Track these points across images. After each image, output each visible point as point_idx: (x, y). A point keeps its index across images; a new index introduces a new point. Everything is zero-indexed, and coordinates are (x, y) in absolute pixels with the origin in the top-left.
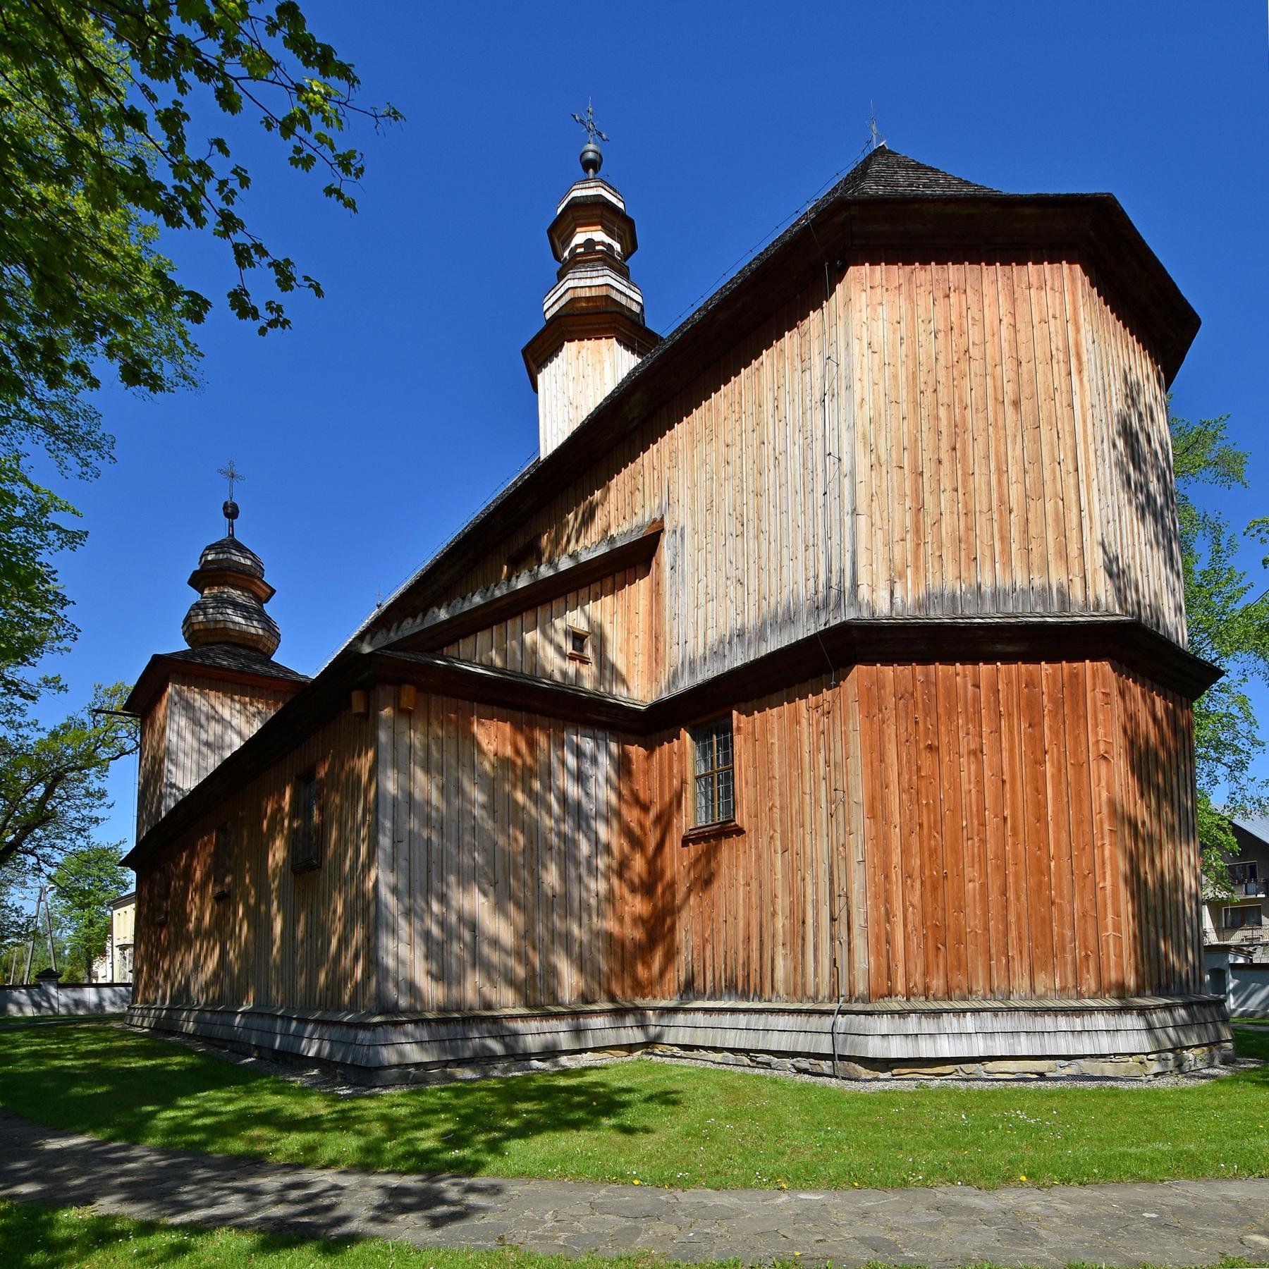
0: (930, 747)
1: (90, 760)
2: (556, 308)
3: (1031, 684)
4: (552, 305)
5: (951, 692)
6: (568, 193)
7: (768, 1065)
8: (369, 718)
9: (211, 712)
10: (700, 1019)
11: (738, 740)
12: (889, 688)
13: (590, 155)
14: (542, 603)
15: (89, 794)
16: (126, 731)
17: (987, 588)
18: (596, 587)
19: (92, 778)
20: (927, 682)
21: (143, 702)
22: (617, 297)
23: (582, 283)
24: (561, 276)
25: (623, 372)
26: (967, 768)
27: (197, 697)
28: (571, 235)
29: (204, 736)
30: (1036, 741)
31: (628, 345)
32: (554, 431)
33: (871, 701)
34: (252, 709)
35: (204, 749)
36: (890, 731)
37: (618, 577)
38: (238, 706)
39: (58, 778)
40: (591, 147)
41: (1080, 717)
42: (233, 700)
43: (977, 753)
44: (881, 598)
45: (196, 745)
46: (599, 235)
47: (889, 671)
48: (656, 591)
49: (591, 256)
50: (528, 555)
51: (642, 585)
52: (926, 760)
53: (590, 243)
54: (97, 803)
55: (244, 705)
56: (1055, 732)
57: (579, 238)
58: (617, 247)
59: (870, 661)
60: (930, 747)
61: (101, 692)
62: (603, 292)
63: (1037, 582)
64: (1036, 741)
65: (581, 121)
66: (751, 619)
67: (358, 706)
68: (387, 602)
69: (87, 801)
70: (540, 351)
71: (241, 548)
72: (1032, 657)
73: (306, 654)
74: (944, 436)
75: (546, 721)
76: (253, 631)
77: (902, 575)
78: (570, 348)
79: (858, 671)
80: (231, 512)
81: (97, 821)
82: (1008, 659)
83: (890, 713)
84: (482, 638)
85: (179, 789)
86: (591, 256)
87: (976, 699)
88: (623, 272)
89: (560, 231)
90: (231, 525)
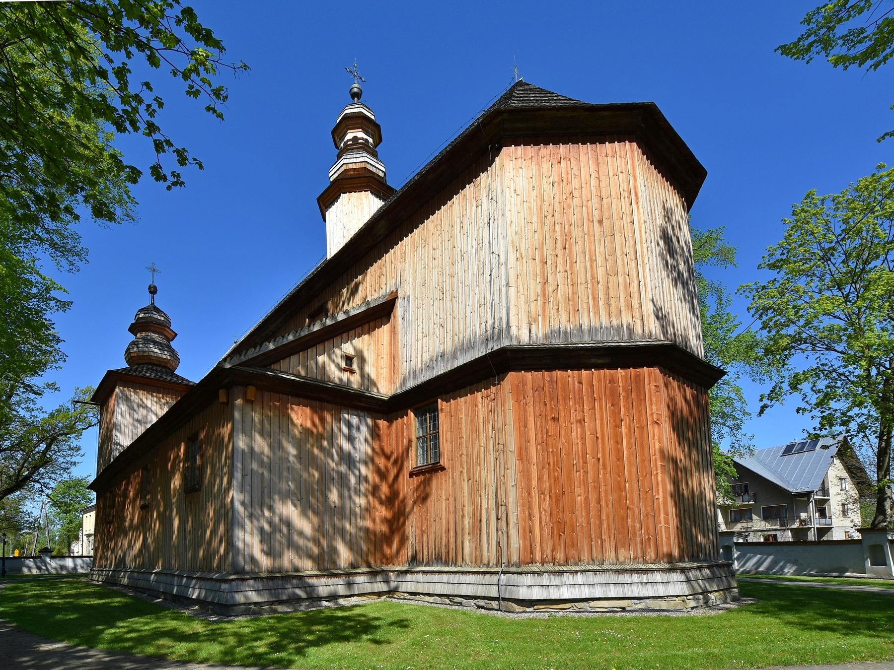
0: (553, 419)
2: (336, 175)
4: (334, 173)
7: (461, 604)
8: (229, 405)
9: (140, 402)
10: (420, 577)
11: (441, 416)
13: (356, 90)
15: (71, 449)
16: (92, 414)
17: (585, 327)
18: (359, 330)
19: (72, 439)
20: (551, 381)
21: (102, 397)
22: (371, 168)
24: (339, 157)
27: (132, 394)
28: (345, 134)
29: (136, 416)
30: (616, 414)
31: (378, 195)
33: (519, 393)
34: (163, 401)
35: (136, 424)
36: (530, 409)
37: (372, 324)
38: (155, 399)
39: (54, 439)
42: (152, 396)
43: (581, 422)
44: (524, 333)
45: (131, 421)
46: (360, 134)
47: (529, 375)
48: (394, 332)
51: (385, 329)
52: (552, 426)
53: (355, 139)
55: (159, 398)
56: (627, 409)
57: (349, 136)
58: (371, 140)
60: (553, 419)
62: (363, 165)
63: (615, 323)
64: (616, 414)
67: (222, 398)
69: (70, 452)
70: (328, 199)
71: (158, 311)
73: (194, 369)
74: (558, 244)
76: (164, 357)
77: (536, 320)
78: (344, 197)
79: (511, 376)
80: (153, 290)
81: (75, 464)
82: (598, 367)
83: (530, 399)
84: (294, 359)
85: (121, 446)
88: (374, 154)
89: (338, 132)
90: (153, 298)
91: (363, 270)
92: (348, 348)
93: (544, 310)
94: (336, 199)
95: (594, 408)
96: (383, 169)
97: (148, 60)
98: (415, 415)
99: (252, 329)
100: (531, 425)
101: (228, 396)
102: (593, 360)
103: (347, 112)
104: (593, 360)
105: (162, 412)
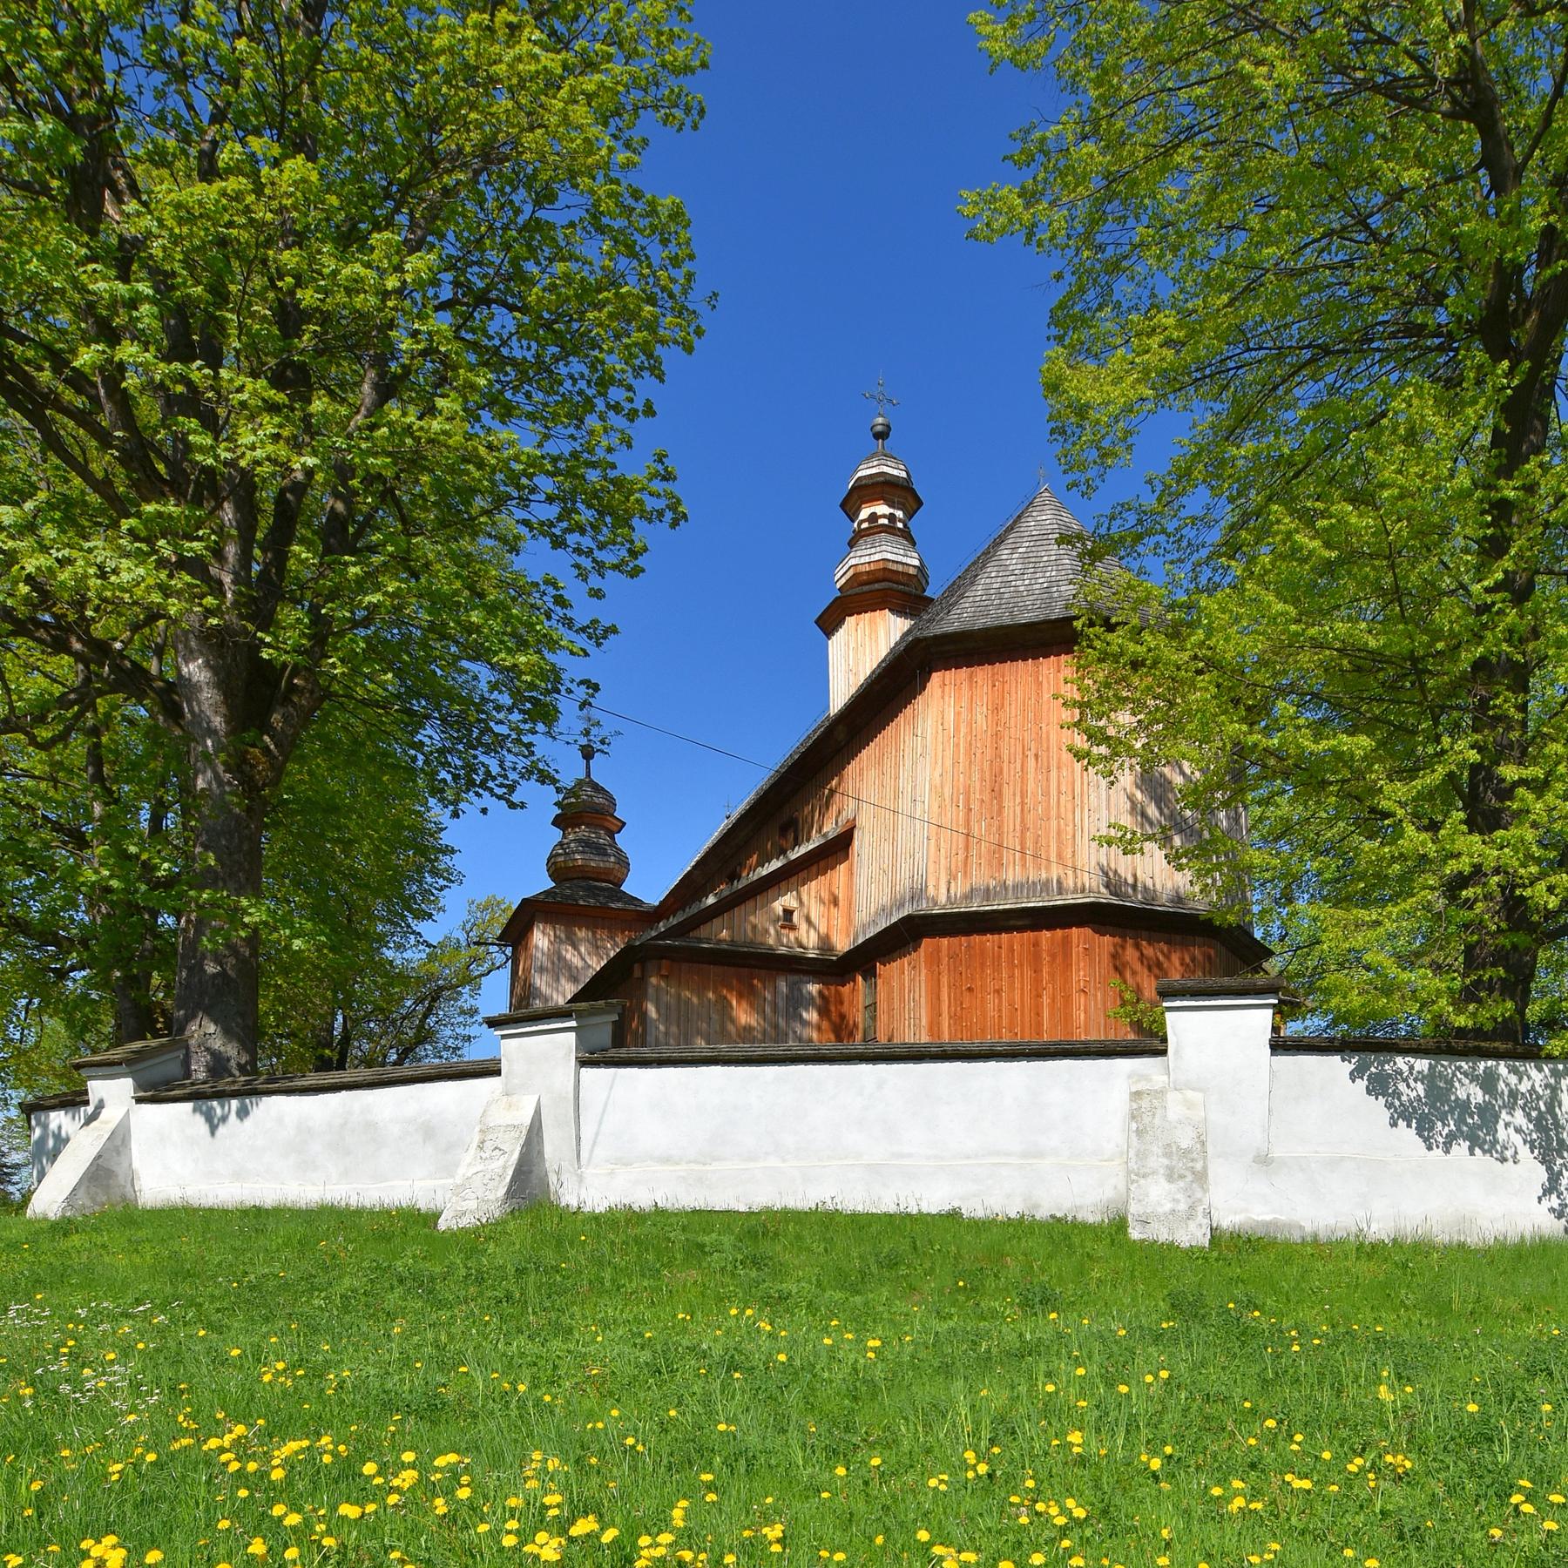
0: (970, 989)
1: (469, 980)
2: (843, 581)
3: (1036, 944)
4: (841, 576)
5: (983, 952)
6: (856, 471)
8: (643, 979)
11: (879, 982)
12: (944, 952)
13: (879, 428)
14: (761, 893)
15: (463, 1012)
16: (498, 955)
17: (1010, 883)
18: (804, 874)
19: (466, 996)
20: (968, 946)
21: (515, 933)
22: (895, 567)
23: (863, 560)
24: (852, 544)
25: (896, 636)
26: (991, 1001)
28: (858, 510)
30: (1037, 981)
31: (899, 611)
32: (840, 693)
33: (934, 960)
36: (944, 980)
37: (822, 864)
39: (435, 996)
40: (880, 420)
41: (1067, 965)
43: (998, 992)
44: (943, 895)
46: (882, 509)
47: (945, 941)
48: (851, 870)
49: (875, 528)
50: (793, 830)
51: (842, 867)
52: (967, 997)
53: (873, 517)
54: (469, 1021)
56: (1052, 975)
57: (865, 513)
58: (899, 514)
59: (932, 936)
60: (970, 989)
61: (474, 908)
62: (881, 565)
63: (1044, 876)
64: (1037, 981)
65: (873, 397)
66: (886, 900)
67: (637, 973)
68: (735, 815)
69: (461, 1019)
70: (829, 622)
71: (597, 788)
72: (1036, 927)
73: (649, 883)
74: (991, 784)
75: (763, 972)
77: (955, 878)
78: (850, 621)
79: (926, 942)
81: (469, 1039)
82: (1020, 929)
83: (944, 967)
84: (716, 922)
86: (875, 528)
87: (1000, 956)
88: (906, 535)
89: (850, 505)
90: (588, 767)
91: (839, 770)
92: (778, 906)
93: (966, 864)
94: (841, 622)
95: (1012, 976)
96: (916, 563)
97: (543, 783)
98: (865, 979)
99: (716, 835)
100: (945, 997)
101: (643, 971)
102: (1012, 923)
103: (860, 474)
104: (1012, 923)
105: (597, 964)
